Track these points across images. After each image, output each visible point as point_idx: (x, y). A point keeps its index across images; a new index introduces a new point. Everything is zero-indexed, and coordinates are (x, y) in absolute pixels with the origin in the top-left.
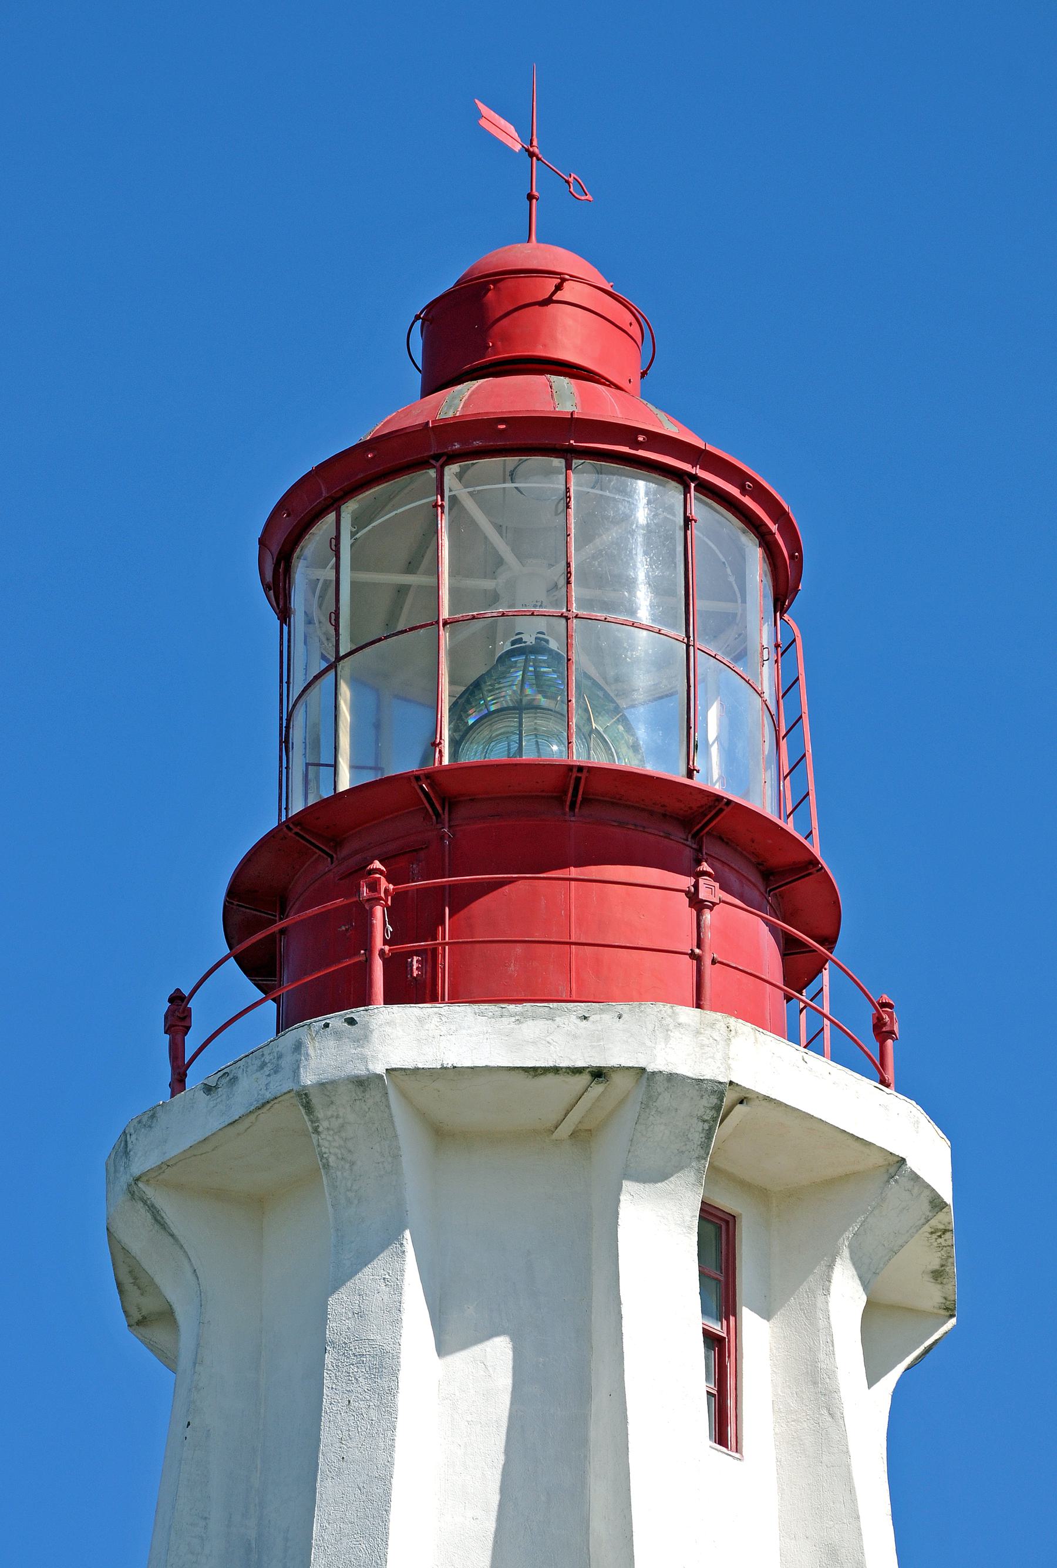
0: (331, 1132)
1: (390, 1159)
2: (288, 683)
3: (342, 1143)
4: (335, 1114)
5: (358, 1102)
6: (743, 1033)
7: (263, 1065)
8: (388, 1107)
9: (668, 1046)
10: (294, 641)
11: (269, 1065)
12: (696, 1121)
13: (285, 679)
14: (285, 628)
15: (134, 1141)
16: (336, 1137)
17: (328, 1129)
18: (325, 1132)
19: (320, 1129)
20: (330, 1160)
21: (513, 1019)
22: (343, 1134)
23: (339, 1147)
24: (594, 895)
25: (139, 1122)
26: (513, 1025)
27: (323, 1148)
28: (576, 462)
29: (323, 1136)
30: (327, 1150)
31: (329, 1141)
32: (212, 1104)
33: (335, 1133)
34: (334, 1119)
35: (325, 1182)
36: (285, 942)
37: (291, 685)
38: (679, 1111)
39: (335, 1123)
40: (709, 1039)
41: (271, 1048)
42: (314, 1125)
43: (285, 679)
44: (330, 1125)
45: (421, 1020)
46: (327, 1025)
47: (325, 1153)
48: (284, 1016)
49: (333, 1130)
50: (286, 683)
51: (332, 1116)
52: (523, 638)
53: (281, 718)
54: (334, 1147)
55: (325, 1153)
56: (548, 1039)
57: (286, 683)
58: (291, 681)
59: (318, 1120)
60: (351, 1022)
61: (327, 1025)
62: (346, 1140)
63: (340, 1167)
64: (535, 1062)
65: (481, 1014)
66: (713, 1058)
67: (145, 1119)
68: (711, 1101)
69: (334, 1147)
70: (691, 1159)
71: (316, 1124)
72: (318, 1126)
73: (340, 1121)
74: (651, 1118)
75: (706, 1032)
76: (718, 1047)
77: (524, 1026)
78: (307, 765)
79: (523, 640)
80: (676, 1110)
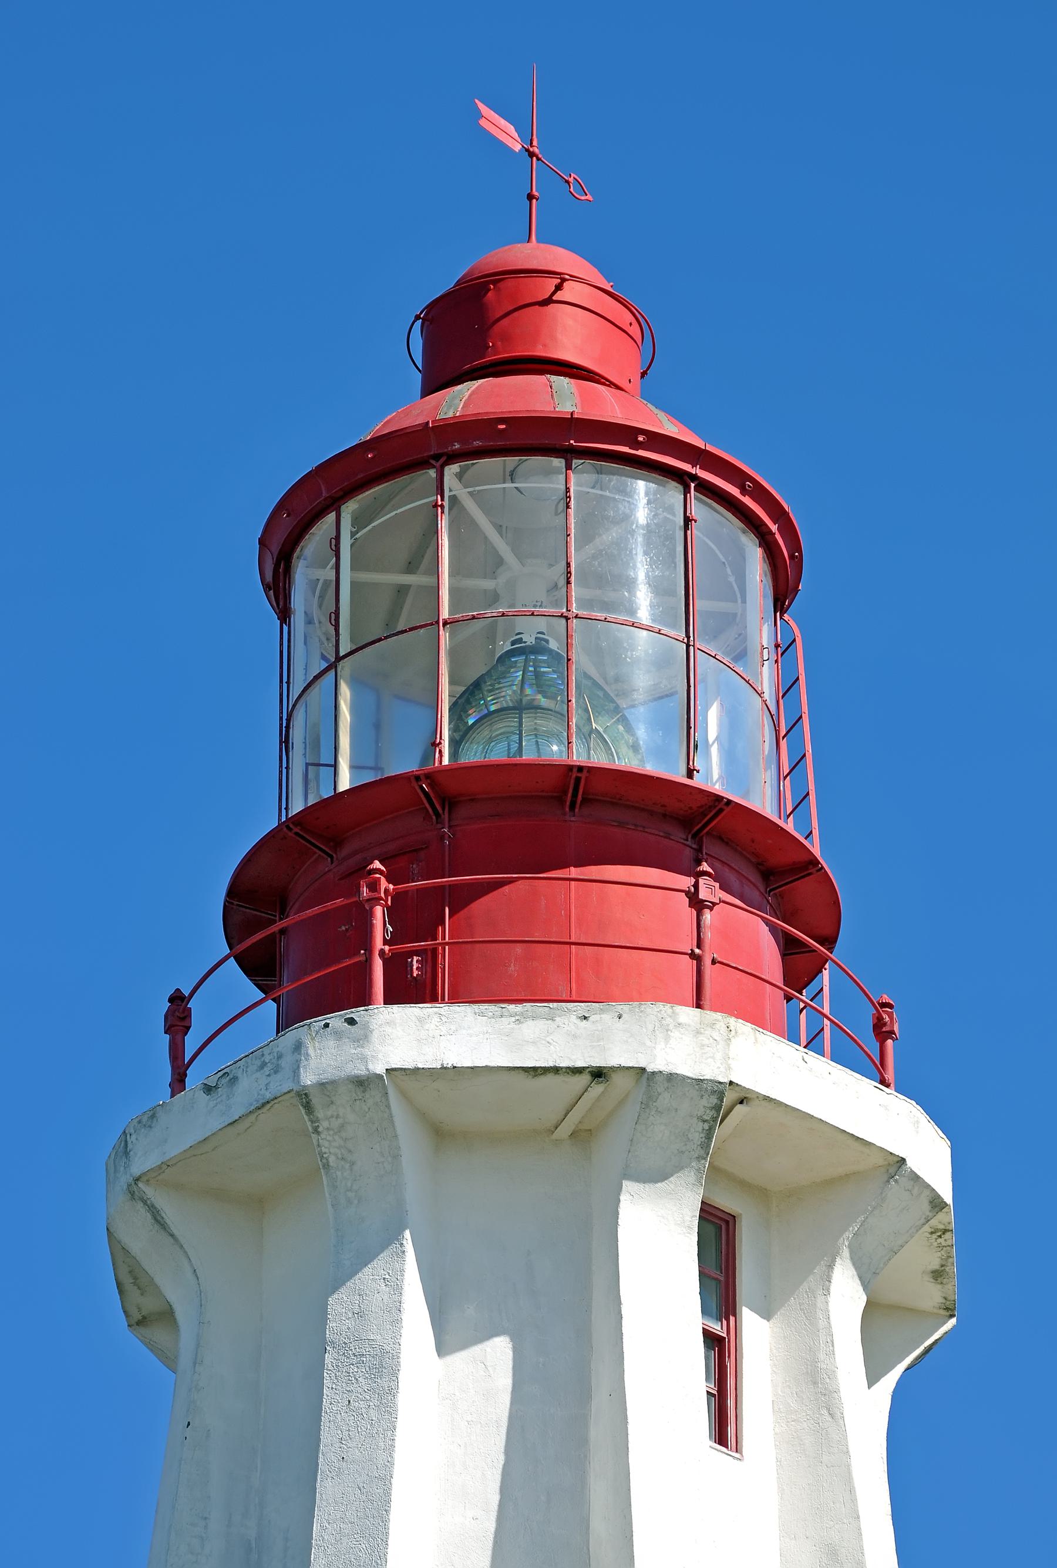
0: (331, 1132)
2: (288, 683)
4: (335, 1114)
5: (358, 1102)
6: (743, 1033)
7: (263, 1065)
8: (388, 1106)
9: (668, 1046)
11: (269, 1064)
13: (285, 679)
14: (285, 628)
16: (336, 1137)
17: (328, 1129)
18: (325, 1132)
19: (320, 1130)
21: (513, 1019)
23: (339, 1147)
25: (139, 1122)
26: (512, 1025)
29: (323, 1136)
30: (327, 1150)
32: (212, 1104)
33: (335, 1134)
35: (325, 1183)
37: (291, 685)
39: (336, 1123)
40: (709, 1039)
43: (285, 679)
44: (330, 1125)
45: (421, 1020)
46: (327, 1025)
47: (325, 1153)
49: (333, 1130)
50: (286, 683)
51: (332, 1117)
53: (281, 718)
55: (325, 1153)
56: (548, 1039)
57: (286, 683)
58: (291, 681)
59: (318, 1120)
60: (351, 1022)
61: (327, 1025)
62: (346, 1140)
64: (535, 1062)
66: (713, 1057)
70: (691, 1159)
71: (316, 1124)
72: (318, 1126)
73: (340, 1121)
74: (651, 1118)
77: (524, 1026)
78: (307, 765)
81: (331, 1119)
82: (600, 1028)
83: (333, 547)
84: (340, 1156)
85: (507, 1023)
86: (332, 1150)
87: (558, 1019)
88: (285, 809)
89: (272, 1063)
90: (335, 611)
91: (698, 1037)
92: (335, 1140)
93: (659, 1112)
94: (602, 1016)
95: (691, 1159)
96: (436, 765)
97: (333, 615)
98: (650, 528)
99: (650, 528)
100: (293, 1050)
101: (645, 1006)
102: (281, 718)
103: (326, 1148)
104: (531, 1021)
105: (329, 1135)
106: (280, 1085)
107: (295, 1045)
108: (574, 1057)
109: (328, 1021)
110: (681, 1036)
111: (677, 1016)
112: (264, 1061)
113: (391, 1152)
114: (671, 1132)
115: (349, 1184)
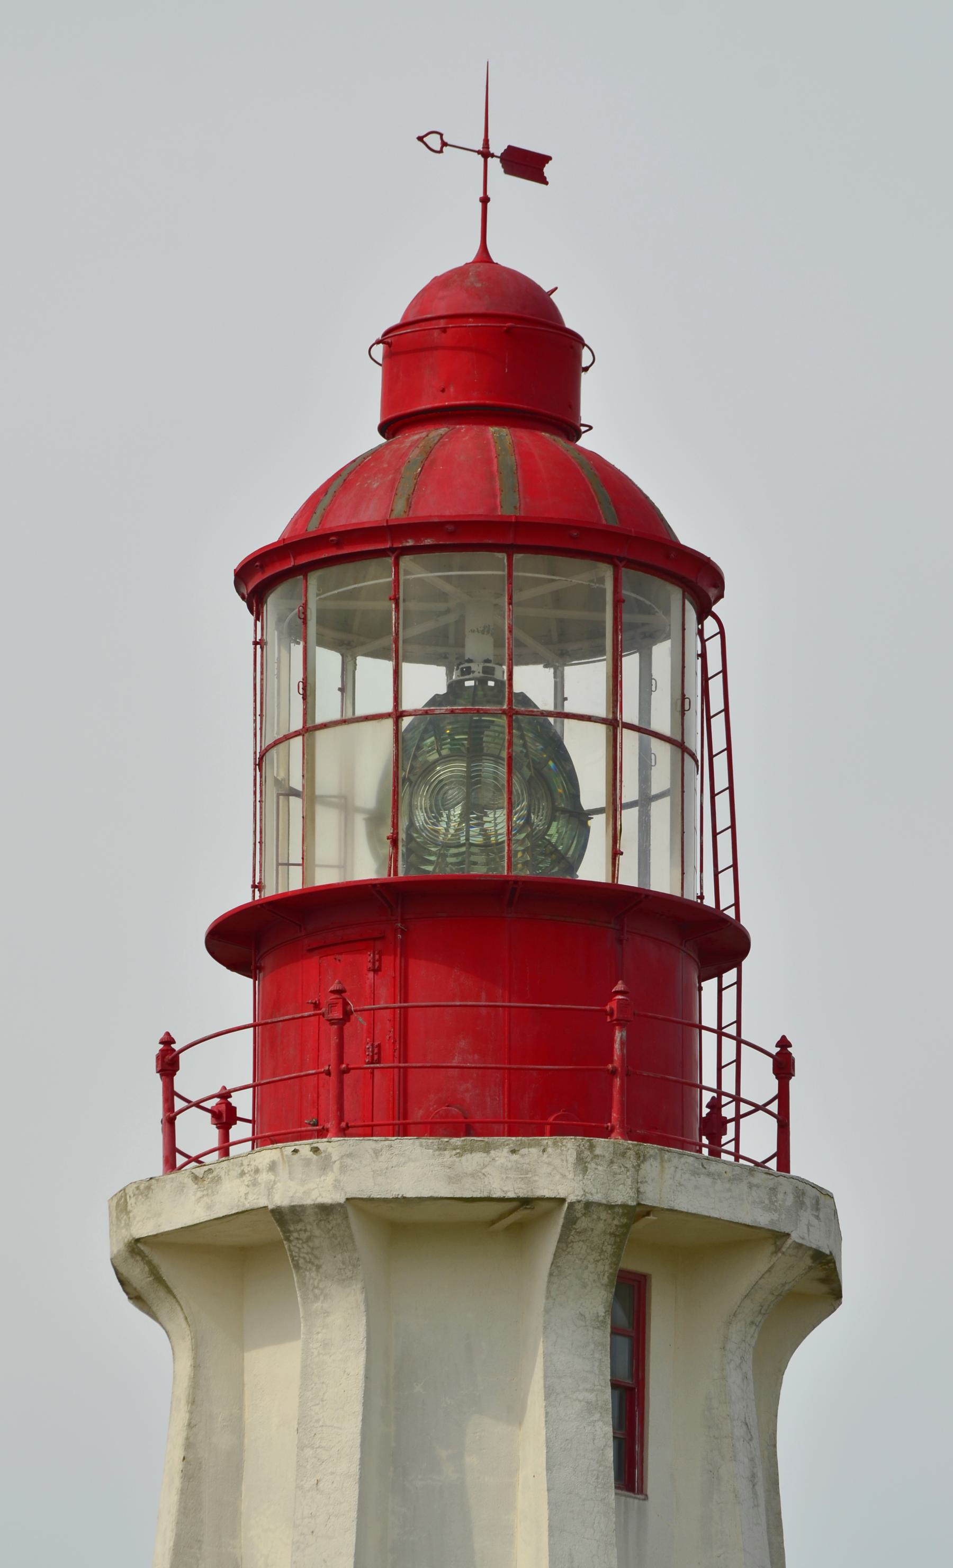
0: (301, 1242)
1: (350, 1267)
2: (261, 715)
3: (309, 1250)
4: (304, 1228)
5: (323, 1222)
6: (651, 1156)
7: (242, 1174)
8: (349, 1227)
9: (586, 1177)
10: (264, 871)
11: (247, 1175)
12: (609, 1237)
13: (258, 712)
14: (259, 624)
15: (133, 1205)
16: (305, 1246)
17: (298, 1239)
18: (296, 1241)
19: (292, 1238)
20: (300, 1262)
21: (454, 1152)
22: (311, 1244)
23: (307, 1253)
24: (527, 989)
25: (138, 1188)
26: (455, 1158)
27: (293, 1253)
28: (517, 557)
29: (294, 1243)
30: (297, 1254)
31: (298, 1248)
32: (199, 1194)
33: (303, 1243)
34: (303, 1232)
35: (295, 1279)
36: (259, 1098)
37: (264, 718)
38: (594, 1231)
39: (304, 1236)
40: (621, 1167)
41: (249, 1160)
42: (286, 1235)
43: (258, 712)
44: (299, 1235)
45: (377, 1153)
46: (296, 1151)
47: (296, 1256)
48: (259, 1064)
49: (301, 1239)
50: (259, 715)
51: (301, 1230)
52: (472, 667)
53: (255, 753)
54: (303, 1253)
55: (296, 1256)
56: (483, 1171)
57: (259, 715)
58: (264, 714)
59: (290, 1231)
60: (316, 1150)
61: (296, 1151)
62: (312, 1249)
63: (308, 1268)
64: (472, 1193)
65: (427, 1147)
66: (624, 1184)
67: (142, 1187)
68: (622, 1220)
69: (303, 1253)
70: (604, 1265)
71: (288, 1234)
72: (289, 1236)
73: (308, 1234)
74: (571, 1237)
75: (619, 1161)
76: (628, 1173)
77: (463, 1158)
78: (278, 795)
79: (472, 670)
80: (592, 1230)
81: (300, 1232)
82: (528, 1161)
83: (301, 691)
84: (308, 1260)
85: (448, 1157)
86: (302, 1255)
87: (492, 1152)
88: (259, 842)
89: (250, 1175)
90: (303, 679)
91: (612, 1166)
92: (303, 1248)
93: (579, 1233)
94: (530, 1149)
95: (604, 1265)
96: (392, 876)
97: (301, 684)
98: (595, 580)
99: (595, 580)
100: (267, 1168)
101: (567, 1141)
102: (255, 753)
103: (296, 1252)
104: (469, 1155)
105: (299, 1243)
106: (258, 1199)
107: (269, 1165)
108: (505, 1189)
109: (297, 1147)
110: (596, 1167)
111: (594, 1149)
112: (243, 1170)
113: (352, 1262)
114: (587, 1246)
115: (316, 1284)
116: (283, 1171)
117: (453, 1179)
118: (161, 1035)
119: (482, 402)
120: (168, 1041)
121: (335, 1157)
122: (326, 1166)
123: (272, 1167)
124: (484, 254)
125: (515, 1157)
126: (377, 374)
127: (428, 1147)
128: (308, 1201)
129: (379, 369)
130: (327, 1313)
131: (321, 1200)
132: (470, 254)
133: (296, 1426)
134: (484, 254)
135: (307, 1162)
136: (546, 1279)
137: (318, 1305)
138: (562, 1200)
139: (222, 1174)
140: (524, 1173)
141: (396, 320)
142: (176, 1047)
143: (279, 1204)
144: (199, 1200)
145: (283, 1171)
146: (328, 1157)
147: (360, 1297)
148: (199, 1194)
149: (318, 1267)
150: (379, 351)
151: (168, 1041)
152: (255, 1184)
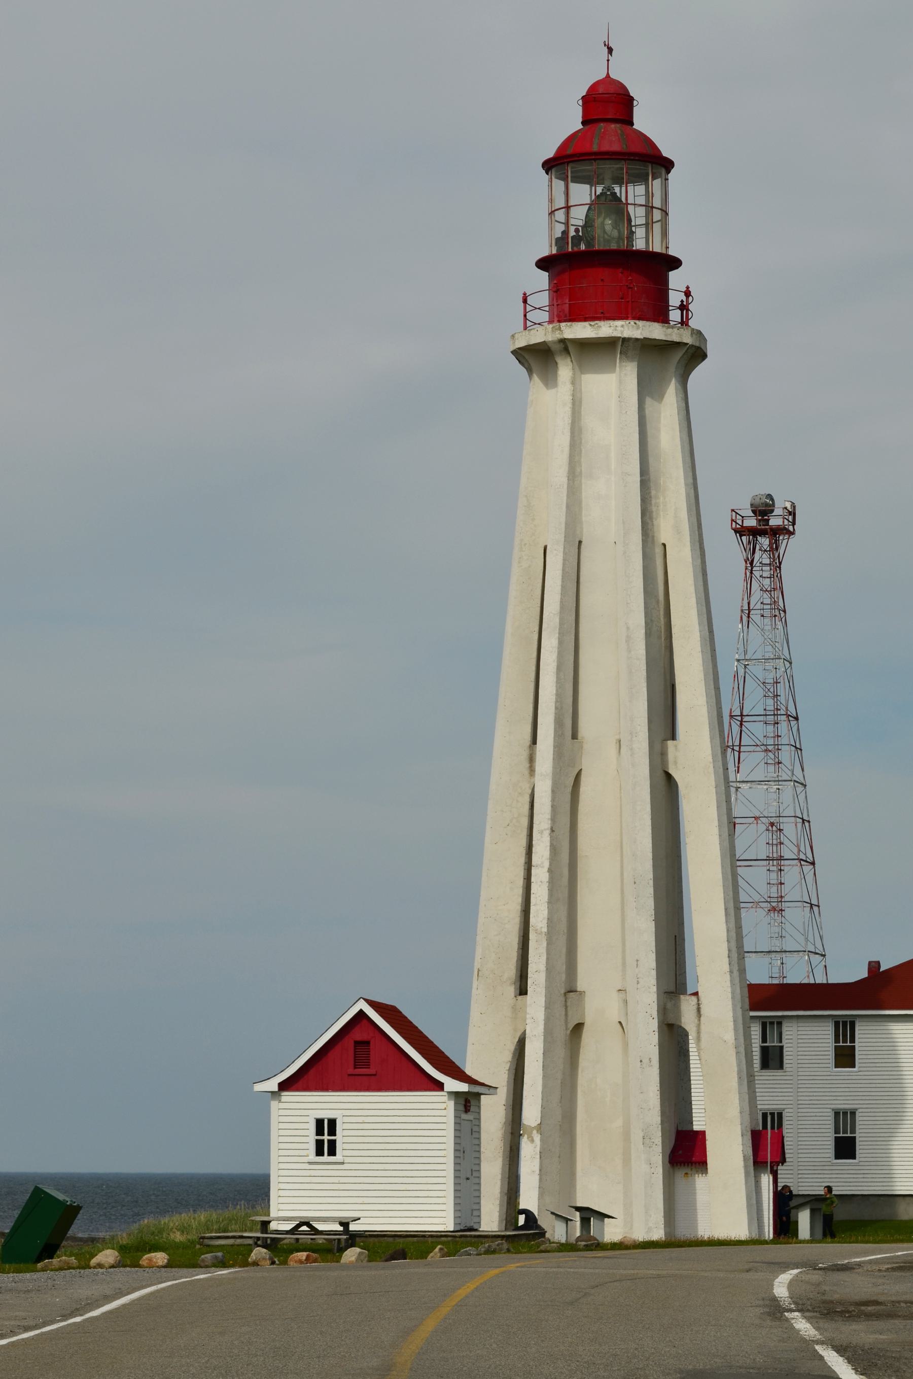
46: (629, 323)
61: (629, 323)
116: (626, 328)
117: (666, 335)
118: (523, 292)
119: (614, 117)
120: (525, 294)
121: (640, 326)
122: (638, 328)
123: (622, 326)
124: (608, 75)
125: (678, 331)
126: (580, 109)
127: (660, 326)
128: (633, 337)
129: (581, 107)
130: (626, 366)
131: (637, 337)
132: (604, 76)
133: (761, 494)
134: (608, 75)
135: (633, 326)
136: (677, 361)
137: (624, 364)
138: (688, 344)
139: (602, 325)
140: (681, 336)
141: (585, 94)
142: (527, 295)
143: (625, 336)
144: (592, 331)
145: (626, 328)
146: (639, 325)
147: (636, 363)
148: (592, 330)
149: (627, 354)
150: (580, 102)
151: (525, 294)
152: (616, 330)
